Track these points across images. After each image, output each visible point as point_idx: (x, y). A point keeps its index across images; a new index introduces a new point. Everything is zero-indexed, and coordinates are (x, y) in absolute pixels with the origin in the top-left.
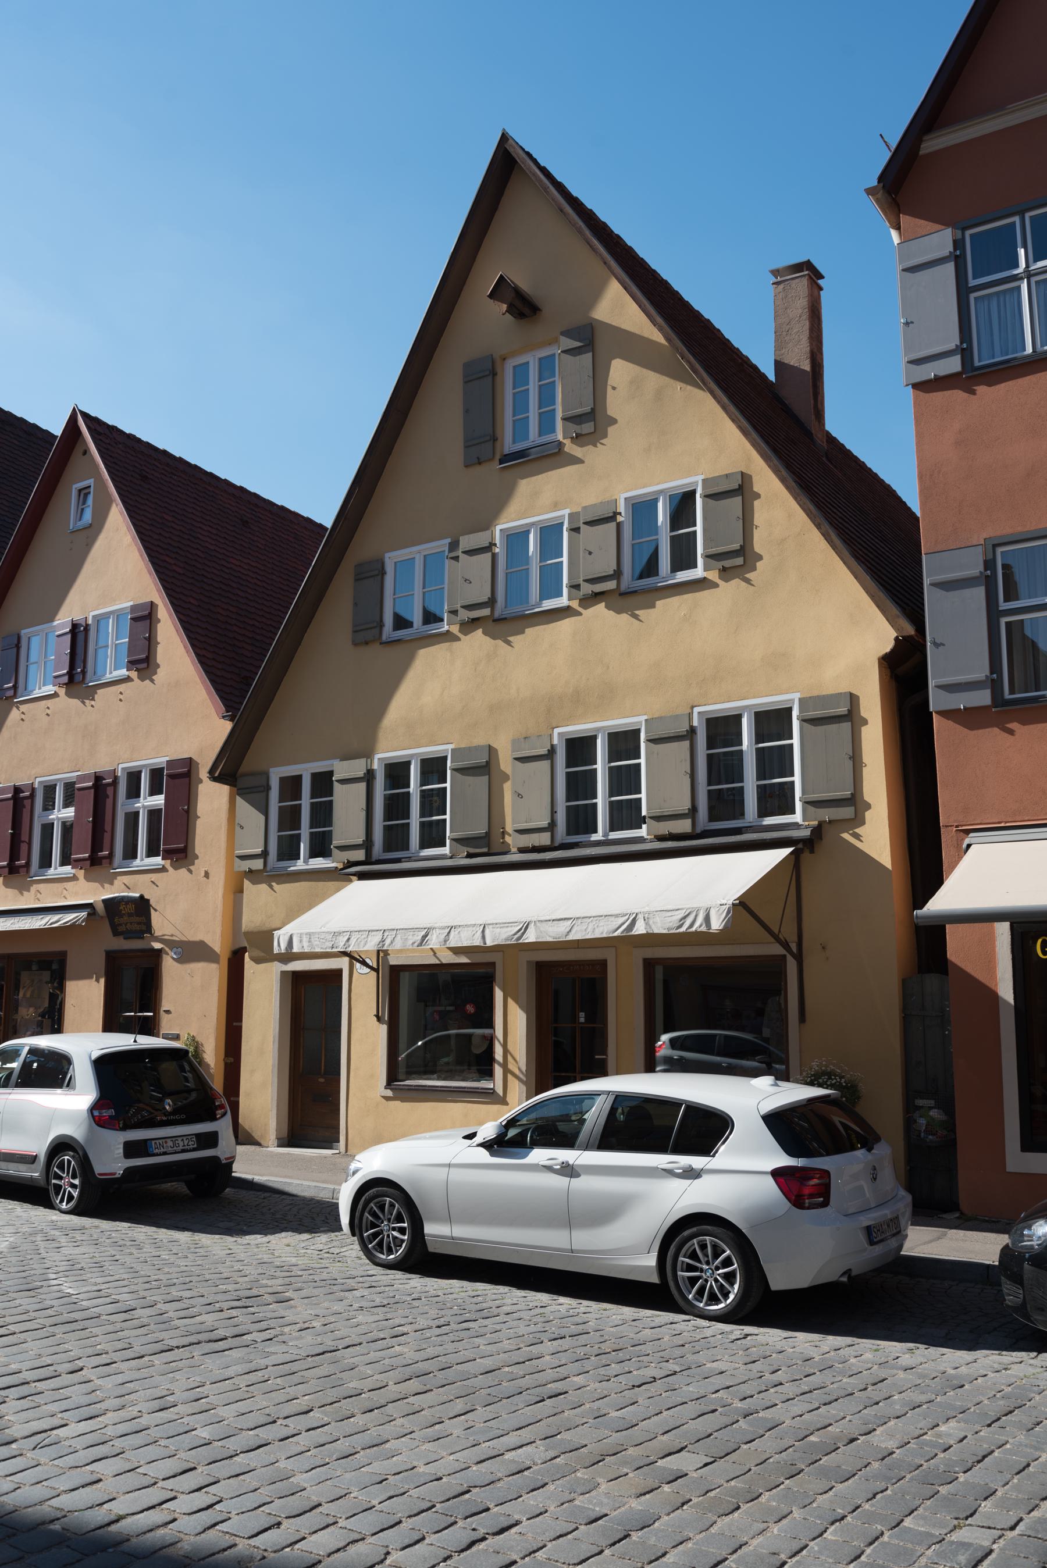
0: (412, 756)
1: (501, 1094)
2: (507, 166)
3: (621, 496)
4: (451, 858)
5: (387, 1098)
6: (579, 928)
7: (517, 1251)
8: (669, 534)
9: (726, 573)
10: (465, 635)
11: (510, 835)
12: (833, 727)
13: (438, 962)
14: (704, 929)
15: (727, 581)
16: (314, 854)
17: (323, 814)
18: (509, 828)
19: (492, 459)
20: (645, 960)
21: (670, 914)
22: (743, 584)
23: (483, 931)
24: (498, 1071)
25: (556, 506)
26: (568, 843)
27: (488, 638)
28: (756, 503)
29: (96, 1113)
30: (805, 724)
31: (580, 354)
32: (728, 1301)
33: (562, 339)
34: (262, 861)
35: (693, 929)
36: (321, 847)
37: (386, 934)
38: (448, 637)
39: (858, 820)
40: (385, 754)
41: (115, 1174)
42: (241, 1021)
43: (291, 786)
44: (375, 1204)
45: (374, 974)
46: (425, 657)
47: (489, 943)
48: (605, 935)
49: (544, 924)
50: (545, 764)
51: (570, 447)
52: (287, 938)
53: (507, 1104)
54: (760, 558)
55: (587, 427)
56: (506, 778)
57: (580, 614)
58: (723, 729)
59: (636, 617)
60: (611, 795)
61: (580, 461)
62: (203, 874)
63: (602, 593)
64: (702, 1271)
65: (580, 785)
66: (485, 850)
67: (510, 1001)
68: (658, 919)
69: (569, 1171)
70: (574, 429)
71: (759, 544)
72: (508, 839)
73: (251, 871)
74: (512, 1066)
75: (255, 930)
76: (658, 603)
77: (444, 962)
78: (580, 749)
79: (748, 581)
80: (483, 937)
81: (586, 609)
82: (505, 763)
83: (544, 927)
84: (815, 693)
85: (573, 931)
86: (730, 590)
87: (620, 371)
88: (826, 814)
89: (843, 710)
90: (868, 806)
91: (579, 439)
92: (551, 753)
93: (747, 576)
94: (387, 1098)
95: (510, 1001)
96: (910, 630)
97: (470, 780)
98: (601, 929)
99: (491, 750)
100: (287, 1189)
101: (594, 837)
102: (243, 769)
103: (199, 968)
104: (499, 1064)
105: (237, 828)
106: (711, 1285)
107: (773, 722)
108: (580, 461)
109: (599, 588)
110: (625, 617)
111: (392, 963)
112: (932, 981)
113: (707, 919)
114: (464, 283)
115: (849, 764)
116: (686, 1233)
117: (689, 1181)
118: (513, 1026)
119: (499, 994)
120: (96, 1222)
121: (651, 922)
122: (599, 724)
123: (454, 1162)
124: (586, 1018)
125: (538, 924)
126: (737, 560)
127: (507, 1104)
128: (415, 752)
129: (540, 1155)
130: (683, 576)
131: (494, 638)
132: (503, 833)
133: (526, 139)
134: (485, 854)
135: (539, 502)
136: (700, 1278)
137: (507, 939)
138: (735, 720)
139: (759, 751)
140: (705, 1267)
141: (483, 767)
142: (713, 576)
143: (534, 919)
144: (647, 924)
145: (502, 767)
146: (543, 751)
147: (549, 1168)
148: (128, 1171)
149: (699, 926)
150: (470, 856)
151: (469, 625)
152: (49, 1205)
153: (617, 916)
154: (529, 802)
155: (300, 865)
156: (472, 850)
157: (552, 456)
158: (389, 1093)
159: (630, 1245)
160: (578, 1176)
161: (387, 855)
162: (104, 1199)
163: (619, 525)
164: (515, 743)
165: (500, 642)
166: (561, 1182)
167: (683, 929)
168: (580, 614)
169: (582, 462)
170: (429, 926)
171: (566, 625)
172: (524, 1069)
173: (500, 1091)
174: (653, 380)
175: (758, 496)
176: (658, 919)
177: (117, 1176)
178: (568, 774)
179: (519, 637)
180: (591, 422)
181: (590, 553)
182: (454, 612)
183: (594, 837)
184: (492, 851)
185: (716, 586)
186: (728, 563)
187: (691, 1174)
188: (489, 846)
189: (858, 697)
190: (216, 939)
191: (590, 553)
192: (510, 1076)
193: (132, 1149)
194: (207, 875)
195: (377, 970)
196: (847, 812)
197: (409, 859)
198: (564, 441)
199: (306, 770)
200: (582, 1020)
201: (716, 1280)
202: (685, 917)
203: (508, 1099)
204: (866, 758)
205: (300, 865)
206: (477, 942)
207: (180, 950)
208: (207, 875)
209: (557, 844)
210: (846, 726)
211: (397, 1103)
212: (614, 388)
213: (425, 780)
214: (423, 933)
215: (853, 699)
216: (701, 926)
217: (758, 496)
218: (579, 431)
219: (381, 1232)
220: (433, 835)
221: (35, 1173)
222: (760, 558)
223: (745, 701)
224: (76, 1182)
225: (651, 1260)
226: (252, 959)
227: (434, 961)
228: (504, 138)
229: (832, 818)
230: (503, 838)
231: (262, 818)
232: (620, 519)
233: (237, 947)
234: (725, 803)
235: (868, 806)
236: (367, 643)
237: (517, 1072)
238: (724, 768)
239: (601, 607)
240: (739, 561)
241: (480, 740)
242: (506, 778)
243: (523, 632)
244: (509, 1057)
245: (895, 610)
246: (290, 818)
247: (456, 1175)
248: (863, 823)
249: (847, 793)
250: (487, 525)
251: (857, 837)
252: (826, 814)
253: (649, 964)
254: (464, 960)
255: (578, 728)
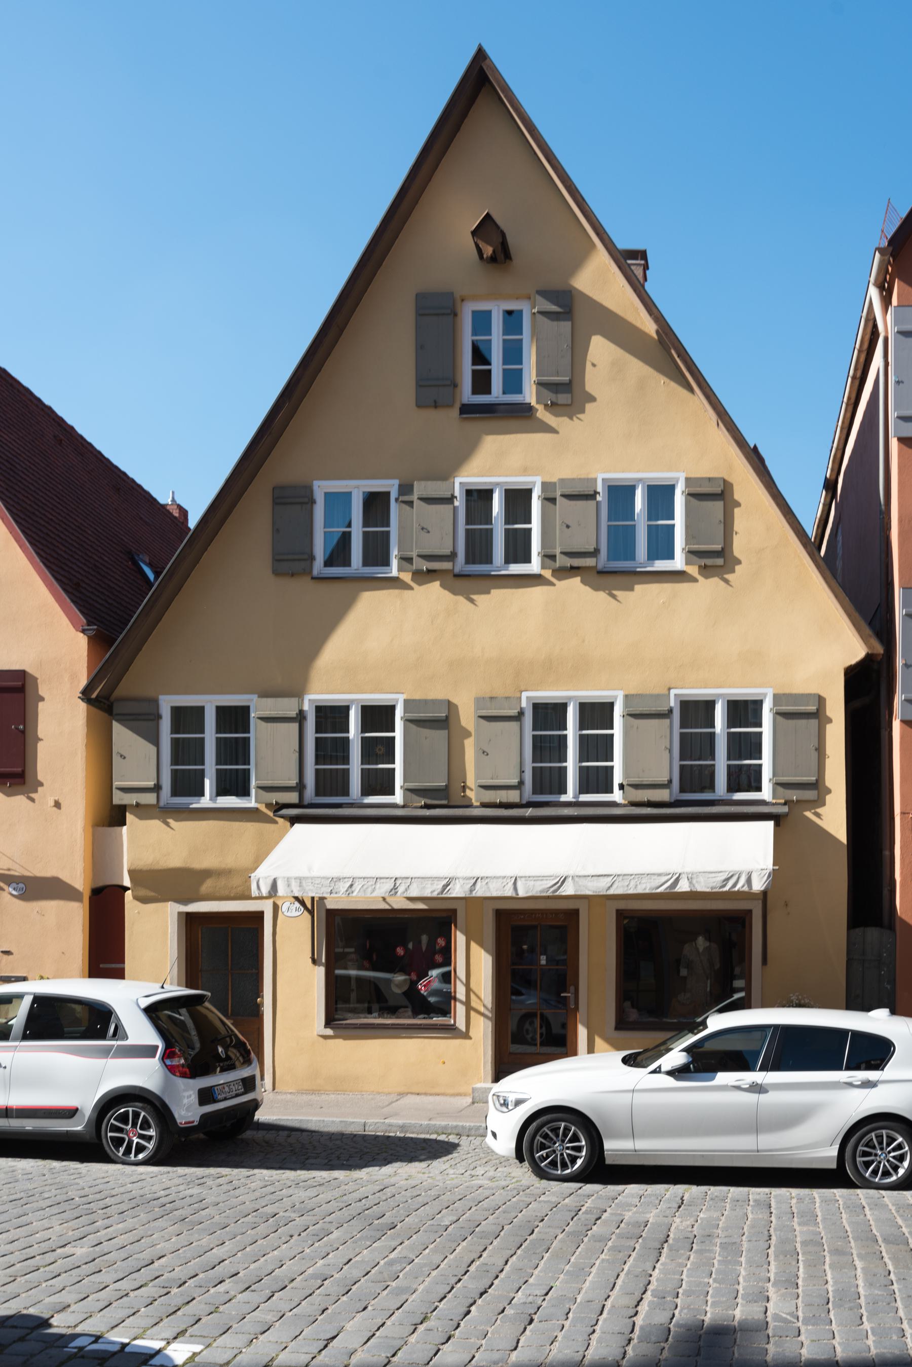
0: (353, 701)
1: (464, 1029)
2: (479, 84)
3: (602, 473)
4: (404, 807)
5: (325, 1037)
6: (620, 884)
7: (703, 1156)
8: (647, 523)
9: (706, 571)
10: (420, 584)
11: (472, 790)
12: (802, 722)
13: (387, 907)
14: (746, 889)
15: (706, 577)
16: (222, 791)
17: (235, 751)
18: (471, 781)
19: (450, 406)
20: (617, 911)
21: (713, 875)
22: (722, 583)
23: (515, 883)
24: (460, 1010)
25: (525, 471)
26: (537, 801)
27: (446, 592)
28: (736, 510)
29: (168, 1062)
30: (778, 717)
31: (558, 319)
32: (900, 1175)
33: (538, 298)
34: (155, 795)
35: (736, 889)
36: (234, 783)
37: (398, 882)
38: (395, 583)
39: (820, 802)
40: (319, 693)
41: (193, 1122)
42: (124, 963)
43: (188, 718)
44: (565, 1126)
45: (307, 916)
46: (369, 602)
47: (522, 893)
48: (647, 891)
49: (582, 879)
50: (514, 725)
51: (542, 413)
52: (270, 882)
53: (470, 1038)
54: (739, 562)
55: (563, 398)
56: (468, 734)
57: (554, 585)
58: (697, 711)
59: (614, 597)
60: (581, 761)
61: (554, 431)
62: (52, 803)
63: (578, 568)
64: (876, 1155)
65: (549, 748)
66: (444, 802)
67: (474, 946)
68: (701, 879)
69: (757, 1088)
70: (549, 397)
71: (739, 547)
72: (468, 793)
73: (138, 805)
74: (475, 1003)
75: (145, 868)
76: (492, 591)
77: (396, 906)
78: (549, 715)
79: (727, 581)
80: (515, 889)
81: (559, 579)
82: (467, 718)
83: (582, 882)
84: (787, 691)
85: (615, 886)
86: (707, 588)
87: (600, 350)
88: (794, 795)
89: (812, 708)
90: (829, 791)
91: (553, 407)
92: (521, 713)
93: (726, 576)
94: (325, 1037)
95: (474, 946)
96: (879, 649)
97: (426, 732)
98: (644, 886)
99: (451, 706)
100: (304, 1126)
101: (564, 798)
102: (119, 692)
103: (52, 907)
104: (461, 1002)
105: (116, 759)
106: (884, 1165)
107: (744, 711)
108: (554, 431)
109: (577, 562)
110: (602, 595)
111: (329, 907)
112: (872, 934)
113: (749, 881)
114: (417, 203)
115: (815, 755)
116: (865, 1129)
117: (868, 1090)
118: (475, 968)
119: (460, 939)
120: (212, 1171)
121: (694, 881)
122: (572, 693)
123: (637, 1087)
124: (547, 960)
125: (577, 879)
126: (715, 559)
127: (470, 1038)
128: (355, 698)
129: (724, 1078)
130: (661, 565)
131: (455, 592)
132: (464, 788)
133: (508, 67)
134: (440, 805)
135: (499, 461)
136: (873, 1162)
137: (541, 891)
138: (709, 705)
139: (730, 735)
140: (879, 1152)
141: (437, 720)
142: (693, 570)
143: (571, 873)
144: (691, 883)
145: (464, 723)
146: (514, 712)
147: (738, 1088)
148: (204, 1117)
149: (741, 886)
150: (427, 806)
151: (424, 576)
152: (106, 1158)
153: (660, 875)
154: (490, 761)
155: (205, 801)
156: (429, 802)
157: (518, 415)
158: (329, 1032)
159: (817, 1144)
160: (766, 1091)
161: (325, 798)
162: (181, 1147)
163: (598, 503)
164: (479, 702)
165: (461, 599)
166: (752, 1097)
167: (726, 889)
168: (553, 584)
169: (556, 432)
170: (450, 876)
171: (537, 593)
172: (489, 1006)
173: (461, 1024)
174: (636, 368)
175: (738, 504)
176: (701, 879)
177: (196, 1123)
178: (534, 736)
179: (483, 596)
180: (566, 394)
181: (568, 527)
182: (409, 560)
183: (564, 798)
184: (452, 804)
185: (695, 580)
186: (709, 562)
187: (868, 1084)
188: (447, 797)
189: (825, 699)
190: (77, 876)
191: (568, 527)
192: (473, 1014)
193: (206, 1096)
194: (57, 805)
195: (311, 912)
196: (810, 795)
197: (351, 805)
198: (537, 406)
199: (210, 703)
200: (543, 962)
201: (888, 1161)
202: (728, 879)
203: (471, 1034)
204: (829, 750)
205: (205, 801)
206: (509, 892)
207: (21, 885)
208: (57, 805)
209: (524, 802)
210: (814, 723)
211: (339, 1042)
212: (594, 365)
213: (366, 726)
214: (445, 882)
215: (821, 700)
216: (743, 886)
217: (738, 504)
218: (554, 400)
219: (554, 1151)
220: (380, 783)
221: (77, 1126)
222: (739, 562)
223: (722, 690)
224: (152, 1132)
225: (834, 1152)
226: (136, 898)
227: (383, 906)
228: (480, 55)
229: (799, 798)
230: (464, 791)
231: (154, 749)
232: (599, 498)
233: (101, 884)
234: (695, 779)
235: (829, 791)
236: (293, 575)
237: (482, 1009)
238: (695, 746)
239: (575, 582)
240: (720, 561)
241: (437, 693)
242: (468, 734)
243: (488, 592)
244: (473, 996)
245: (868, 631)
246: (186, 752)
247: (639, 1098)
248: (824, 804)
249: (813, 779)
250: (446, 475)
251: (818, 815)
252: (794, 795)
253: (621, 914)
254: (421, 906)
255: (549, 694)
